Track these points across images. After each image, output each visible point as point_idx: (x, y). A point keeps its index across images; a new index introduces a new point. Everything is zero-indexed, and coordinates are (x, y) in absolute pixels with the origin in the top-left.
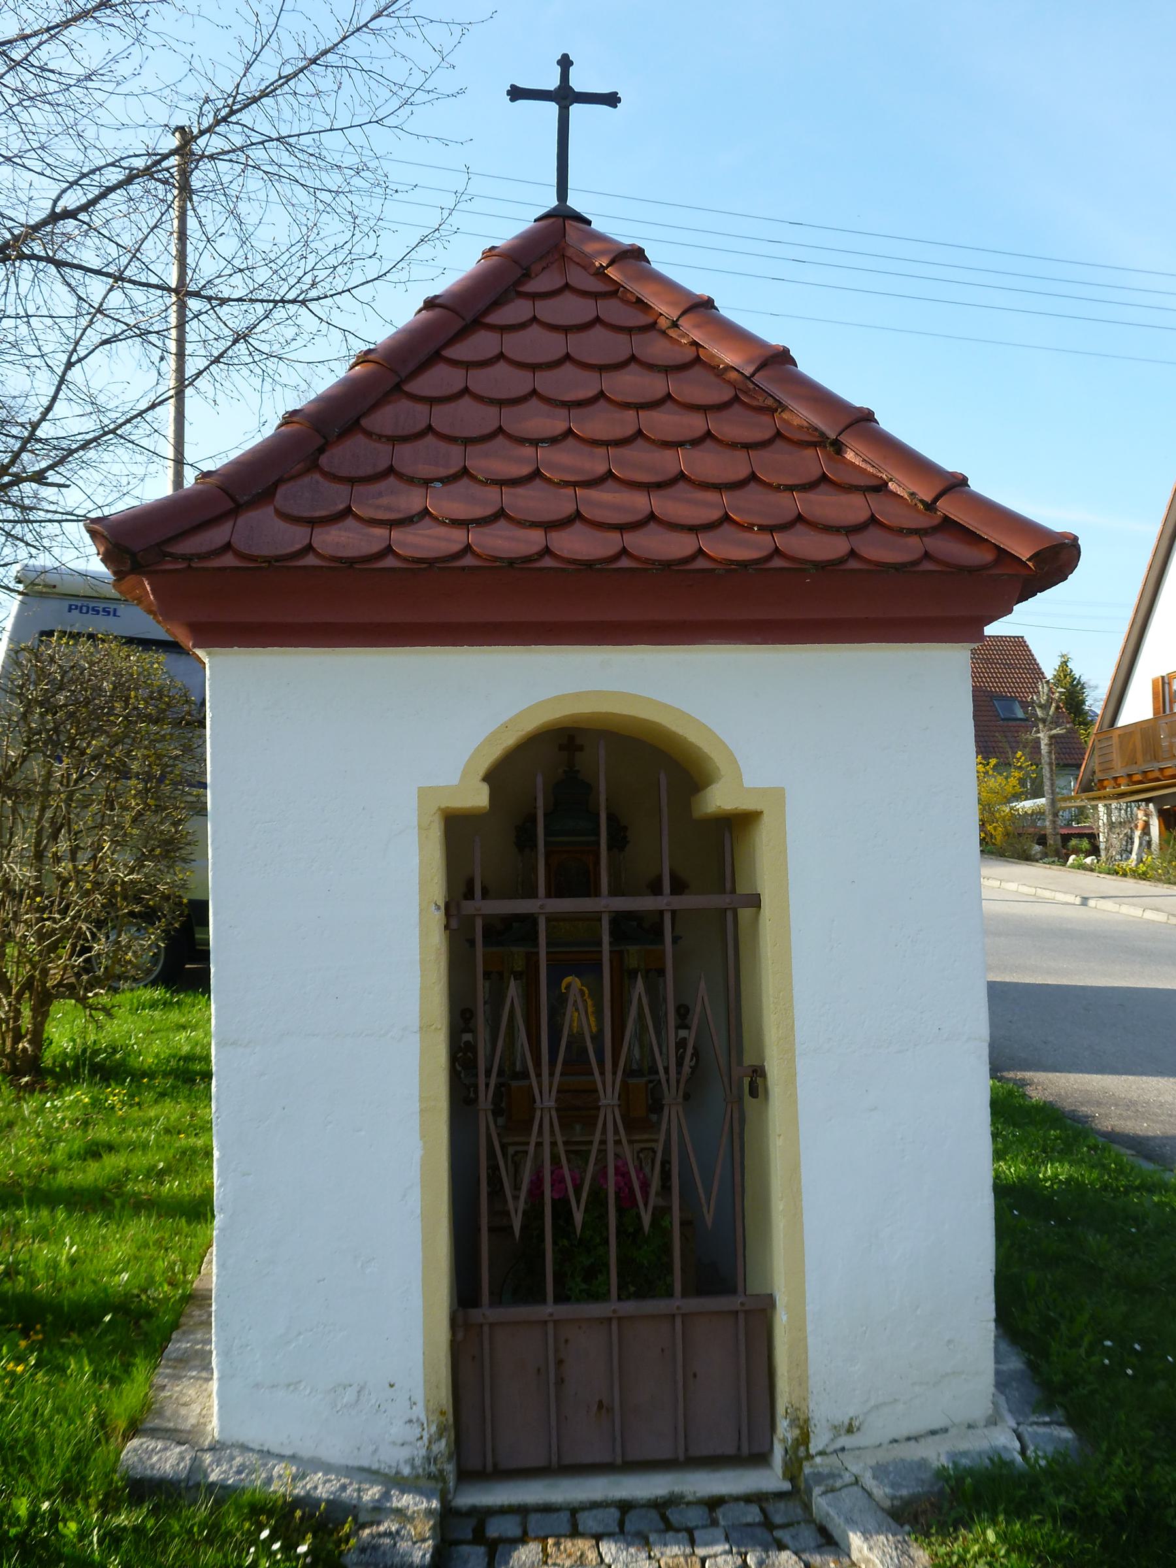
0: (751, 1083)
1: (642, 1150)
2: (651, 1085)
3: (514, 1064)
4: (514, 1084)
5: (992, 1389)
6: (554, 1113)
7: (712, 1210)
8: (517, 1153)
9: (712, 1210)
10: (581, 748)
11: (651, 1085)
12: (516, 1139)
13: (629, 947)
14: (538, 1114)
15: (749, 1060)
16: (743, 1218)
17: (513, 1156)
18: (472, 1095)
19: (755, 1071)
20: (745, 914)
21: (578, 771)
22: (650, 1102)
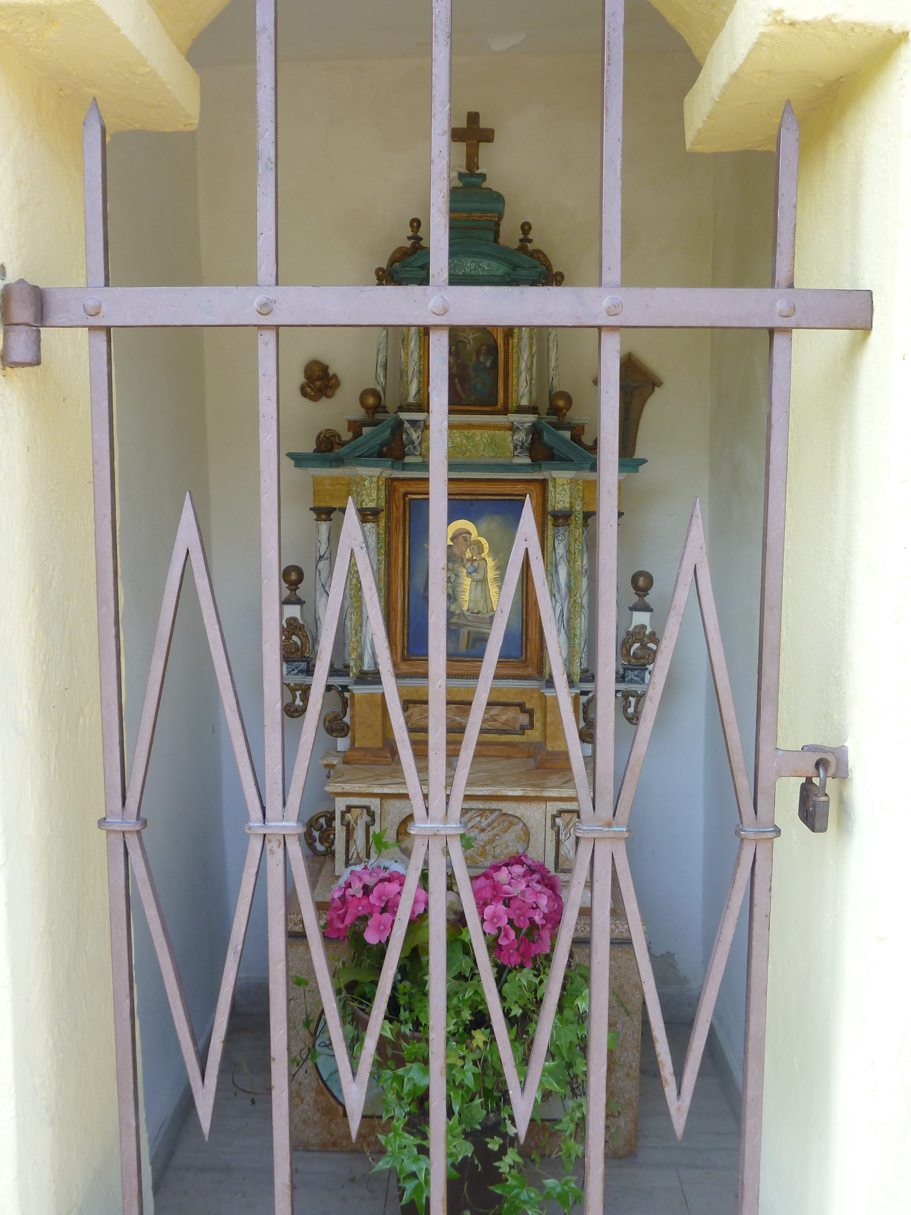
0: (807, 791)
1: (561, 813)
2: (583, 699)
3: (361, 657)
4: (359, 691)
5: (850, 744)
6: (296, 850)
7: (686, 578)
8: (349, 808)
9: (686, 578)
10: (488, 136)
11: (583, 699)
12: (348, 788)
13: (555, 474)
14: (255, 846)
15: (795, 729)
16: (747, 1013)
17: (343, 814)
18: (298, 702)
19: (820, 764)
20: (808, 354)
21: (483, 177)
22: (582, 724)
